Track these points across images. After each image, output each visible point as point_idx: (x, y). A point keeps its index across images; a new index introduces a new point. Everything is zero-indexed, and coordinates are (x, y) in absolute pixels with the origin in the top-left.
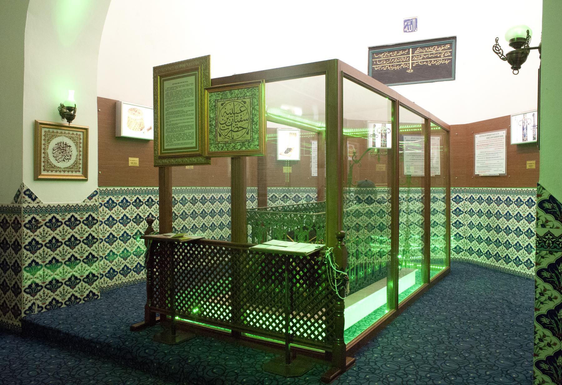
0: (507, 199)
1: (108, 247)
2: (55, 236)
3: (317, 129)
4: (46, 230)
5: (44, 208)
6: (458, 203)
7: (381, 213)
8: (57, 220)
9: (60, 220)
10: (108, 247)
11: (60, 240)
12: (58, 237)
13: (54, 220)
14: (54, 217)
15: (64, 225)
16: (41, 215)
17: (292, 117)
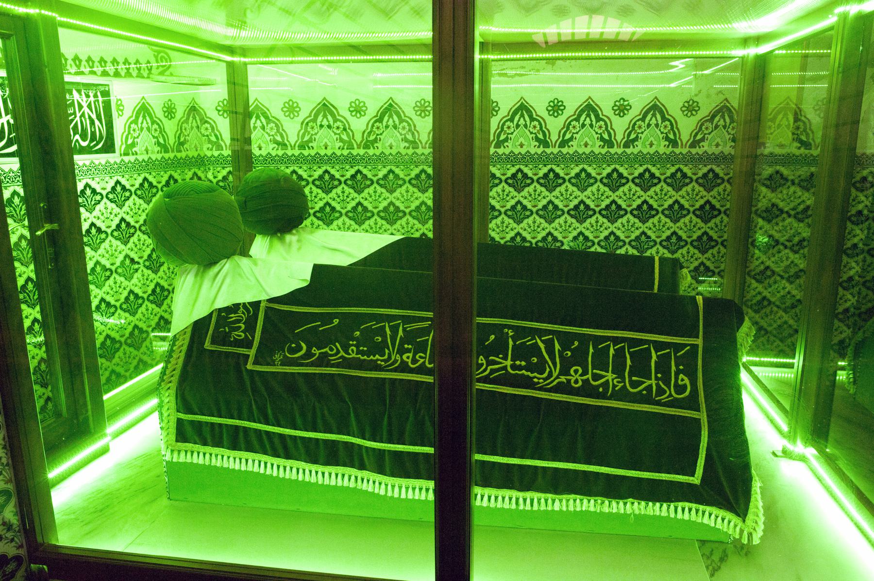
0: (142, 185)
1: (123, 285)
2: (616, 199)
3: (739, 52)
4: (570, 190)
5: (600, 156)
6: (581, 221)
7: (773, 213)
8: (525, 176)
9: (562, 175)
10: (123, 285)
11: (624, 206)
12: (620, 202)
13: (551, 175)
14: (615, 170)
15: (535, 184)
16: (595, 166)
17: (835, 75)
